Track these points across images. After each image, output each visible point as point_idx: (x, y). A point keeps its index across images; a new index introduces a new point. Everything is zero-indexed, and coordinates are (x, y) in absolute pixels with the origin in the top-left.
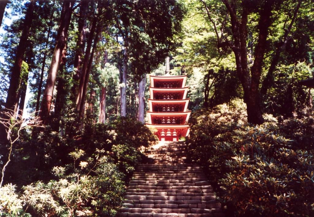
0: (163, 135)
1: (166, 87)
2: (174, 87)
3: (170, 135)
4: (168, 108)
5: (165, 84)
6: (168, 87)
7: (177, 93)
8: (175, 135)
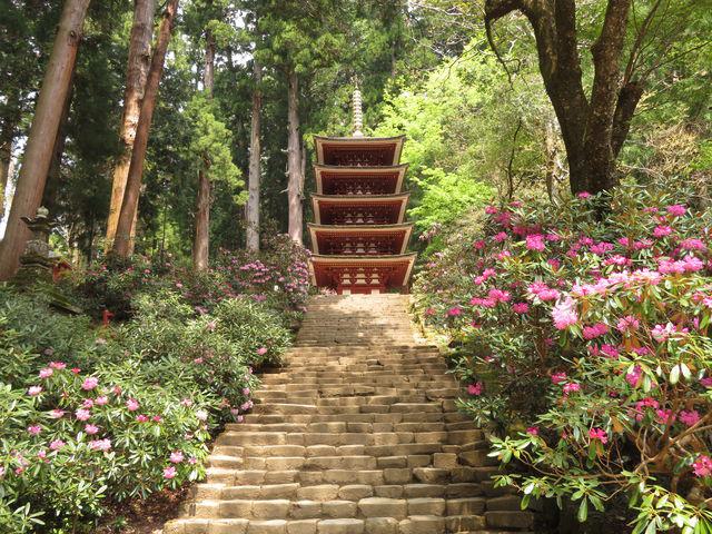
0: (347, 282)
1: (341, 222)
2: (373, 163)
3: (363, 282)
4: (360, 215)
5: (351, 184)
6: (360, 192)
8: (375, 282)
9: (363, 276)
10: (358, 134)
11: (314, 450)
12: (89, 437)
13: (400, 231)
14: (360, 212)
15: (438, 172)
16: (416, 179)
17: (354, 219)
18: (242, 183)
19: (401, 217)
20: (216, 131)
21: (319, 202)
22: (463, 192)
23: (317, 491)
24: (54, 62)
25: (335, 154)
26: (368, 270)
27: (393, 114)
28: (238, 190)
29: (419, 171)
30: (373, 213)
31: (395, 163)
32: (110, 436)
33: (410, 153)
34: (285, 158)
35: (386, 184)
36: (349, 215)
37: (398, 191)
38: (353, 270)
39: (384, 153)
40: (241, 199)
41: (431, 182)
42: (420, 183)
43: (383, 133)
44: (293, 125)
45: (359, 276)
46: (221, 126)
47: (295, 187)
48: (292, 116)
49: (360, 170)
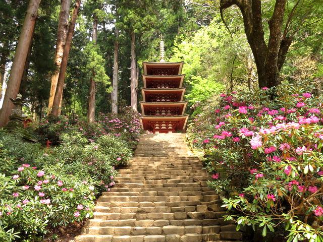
0: (157, 128)
3: (165, 128)
4: (163, 98)
5: (159, 71)
7: (172, 81)
8: (170, 128)
9: (165, 125)
13: (182, 105)
14: (163, 96)
15: (199, 78)
16: (189, 81)
17: (161, 99)
18: (110, 83)
19: (182, 99)
21: (145, 92)
25: (152, 70)
26: (167, 122)
27: (178, 52)
28: (108, 86)
29: (190, 77)
31: (179, 74)
33: (186, 70)
35: (175, 84)
36: (158, 98)
37: (180, 87)
38: (160, 122)
39: (174, 70)
40: (109, 90)
41: (195, 83)
42: (191, 83)
43: (174, 60)
44: (133, 57)
45: (163, 125)
46: (100, 57)
47: (134, 85)
48: (132, 53)
49: (163, 77)
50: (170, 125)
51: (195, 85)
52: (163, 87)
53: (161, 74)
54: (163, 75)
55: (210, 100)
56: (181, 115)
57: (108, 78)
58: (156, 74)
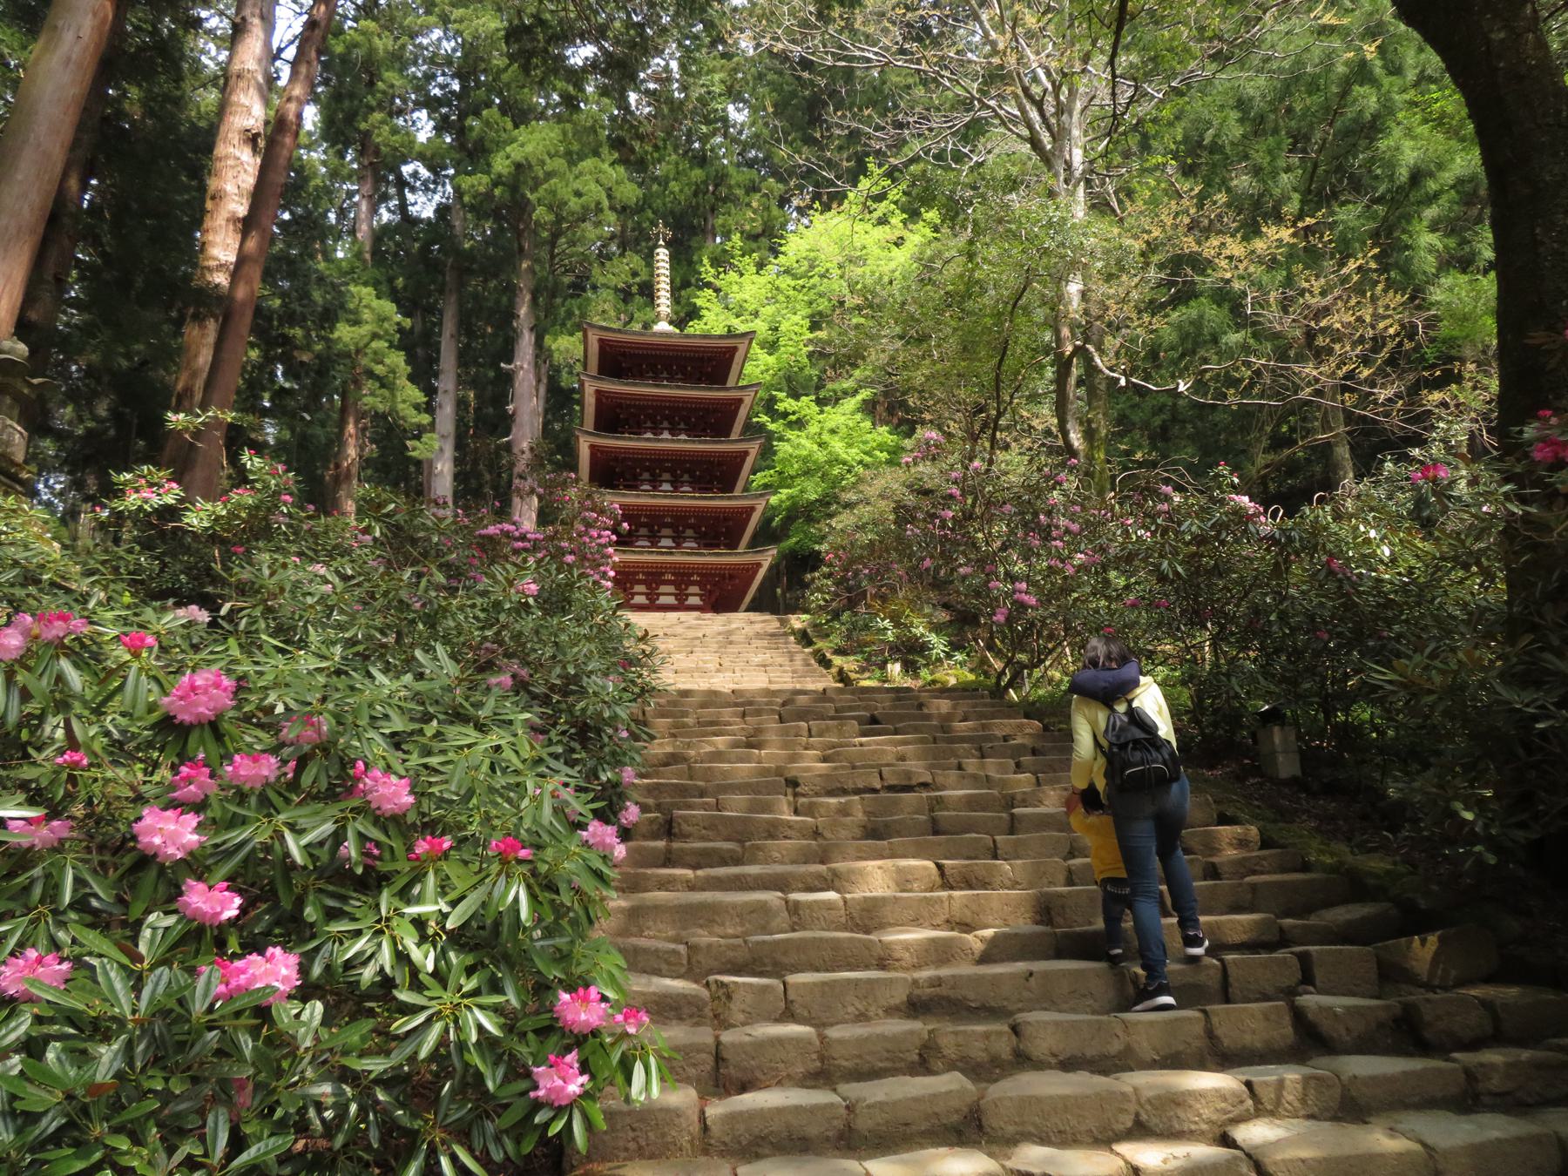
10: (663, 326)
11: (906, 946)
12: (201, 939)
14: (666, 470)
15: (806, 405)
16: (764, 418)
17: (654, 539)
18: (425, 419)
19: (740, 484)
20: (382, 319)
21: (592, 447)
22: (850, 445)
23: (1177, 1100)
24: (60, 23)
25: (618, 359)
27: (717, 308)
28: (419, 432)
29: (772, 400)
30: (690, 472)
31: (731, 383)
32: (292, 930)
33: (758, 366)
34: (508, 379)
35: (717, 419)
36: (646, 476)
39: (715, 361)
40: (417, 449)
41: (790, 425)
42: (772, 427)
43: (713, 321)
45: (663, 589)
46: (388, 307)
50: (694, 589)
51: (790, 434)
52: (666, 487)
53: (657, 430)
54: (666, 435)
55: (851, 496)
56: (731, 489)
57: (418, 396)
58: (637, 429)
